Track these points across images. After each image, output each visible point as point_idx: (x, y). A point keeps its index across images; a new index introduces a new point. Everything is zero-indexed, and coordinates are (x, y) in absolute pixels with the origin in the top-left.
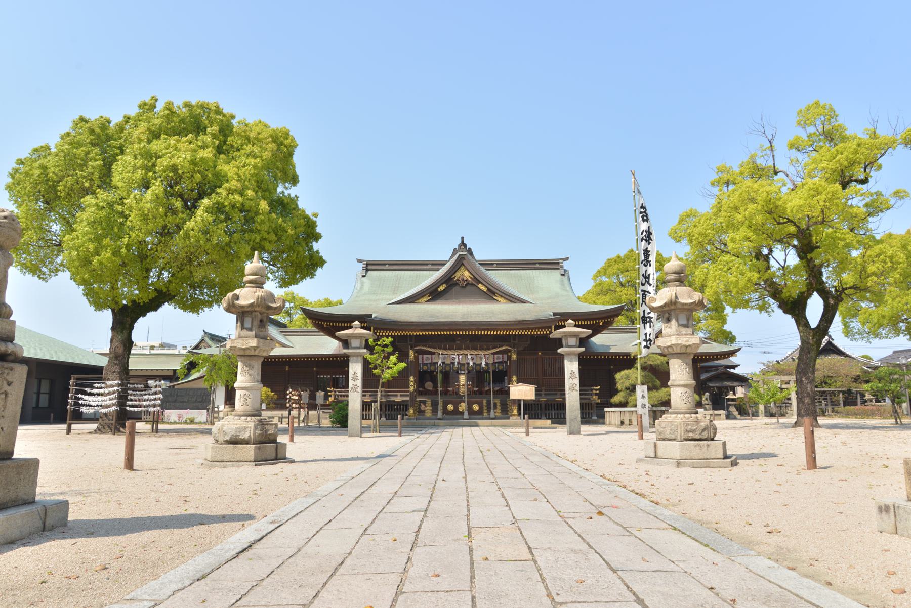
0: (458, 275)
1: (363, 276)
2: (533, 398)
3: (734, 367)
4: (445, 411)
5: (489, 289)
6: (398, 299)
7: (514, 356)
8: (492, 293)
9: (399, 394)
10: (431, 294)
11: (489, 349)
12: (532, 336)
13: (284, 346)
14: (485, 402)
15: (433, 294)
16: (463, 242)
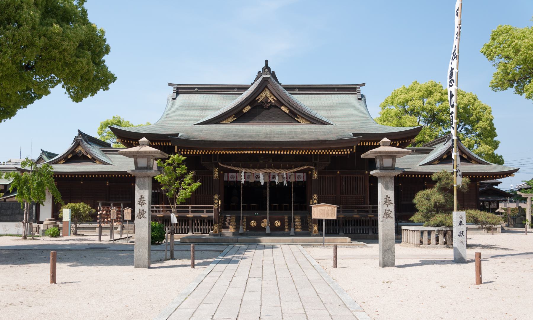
0: (262, 96)
1: (174, 99)
2: (335, 217)
3: (497, 184)
4: (249, 227)
5: (291, 111)
6: (204, 120)
7: (315, 175)
8: (295, 115)
9: (205, 210)
10: (236, 115)
11: (291, 168)
12: (333, 156)
13: (104, 163)
14: (286, 217)
15: (238, 115)
16: (267, 65)
